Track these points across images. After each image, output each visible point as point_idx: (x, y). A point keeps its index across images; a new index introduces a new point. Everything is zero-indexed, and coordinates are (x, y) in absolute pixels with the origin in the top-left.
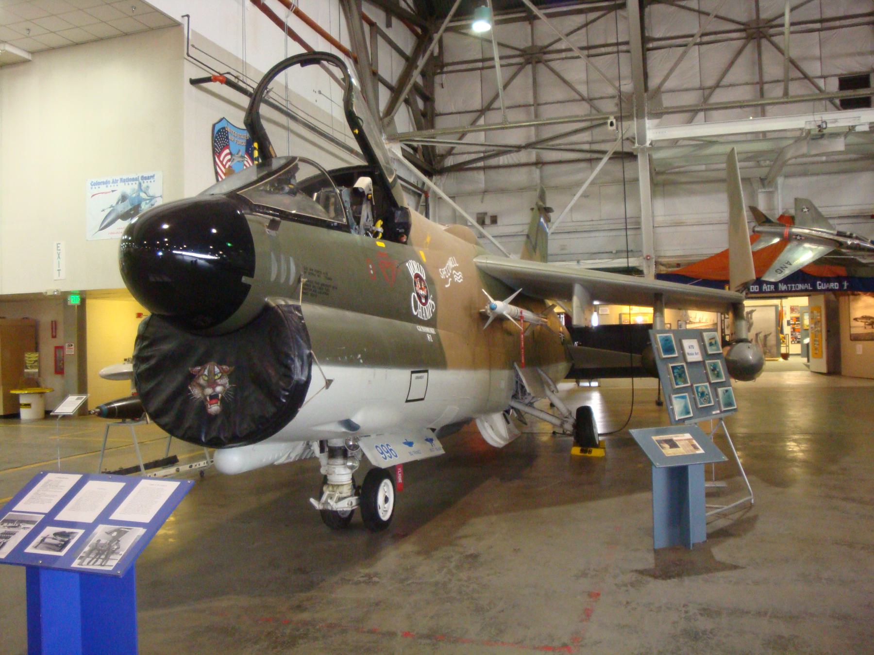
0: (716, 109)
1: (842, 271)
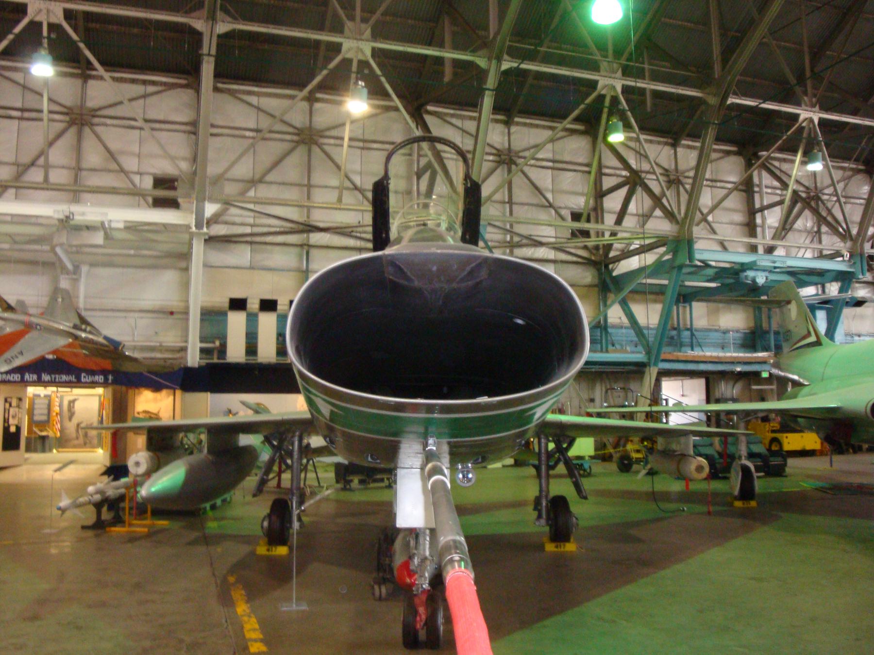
0: (90, 192)
1: (107, 364)
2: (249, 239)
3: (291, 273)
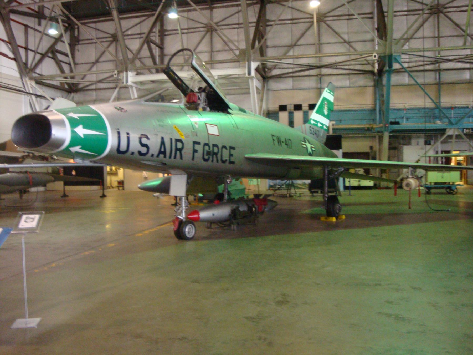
2: (291, 75)
3: (313, 90)
